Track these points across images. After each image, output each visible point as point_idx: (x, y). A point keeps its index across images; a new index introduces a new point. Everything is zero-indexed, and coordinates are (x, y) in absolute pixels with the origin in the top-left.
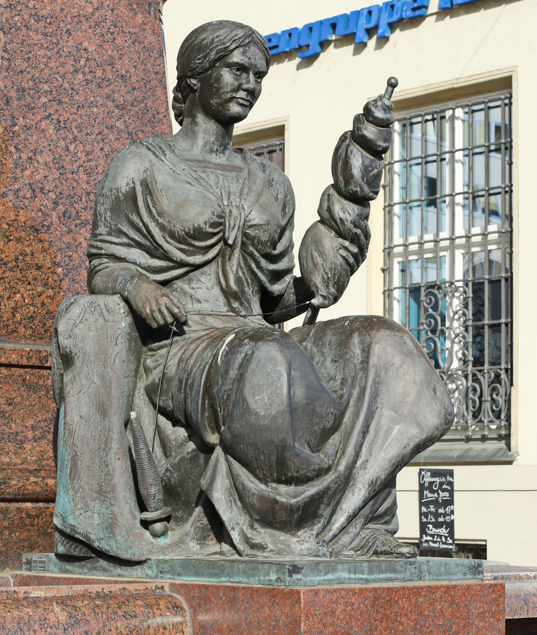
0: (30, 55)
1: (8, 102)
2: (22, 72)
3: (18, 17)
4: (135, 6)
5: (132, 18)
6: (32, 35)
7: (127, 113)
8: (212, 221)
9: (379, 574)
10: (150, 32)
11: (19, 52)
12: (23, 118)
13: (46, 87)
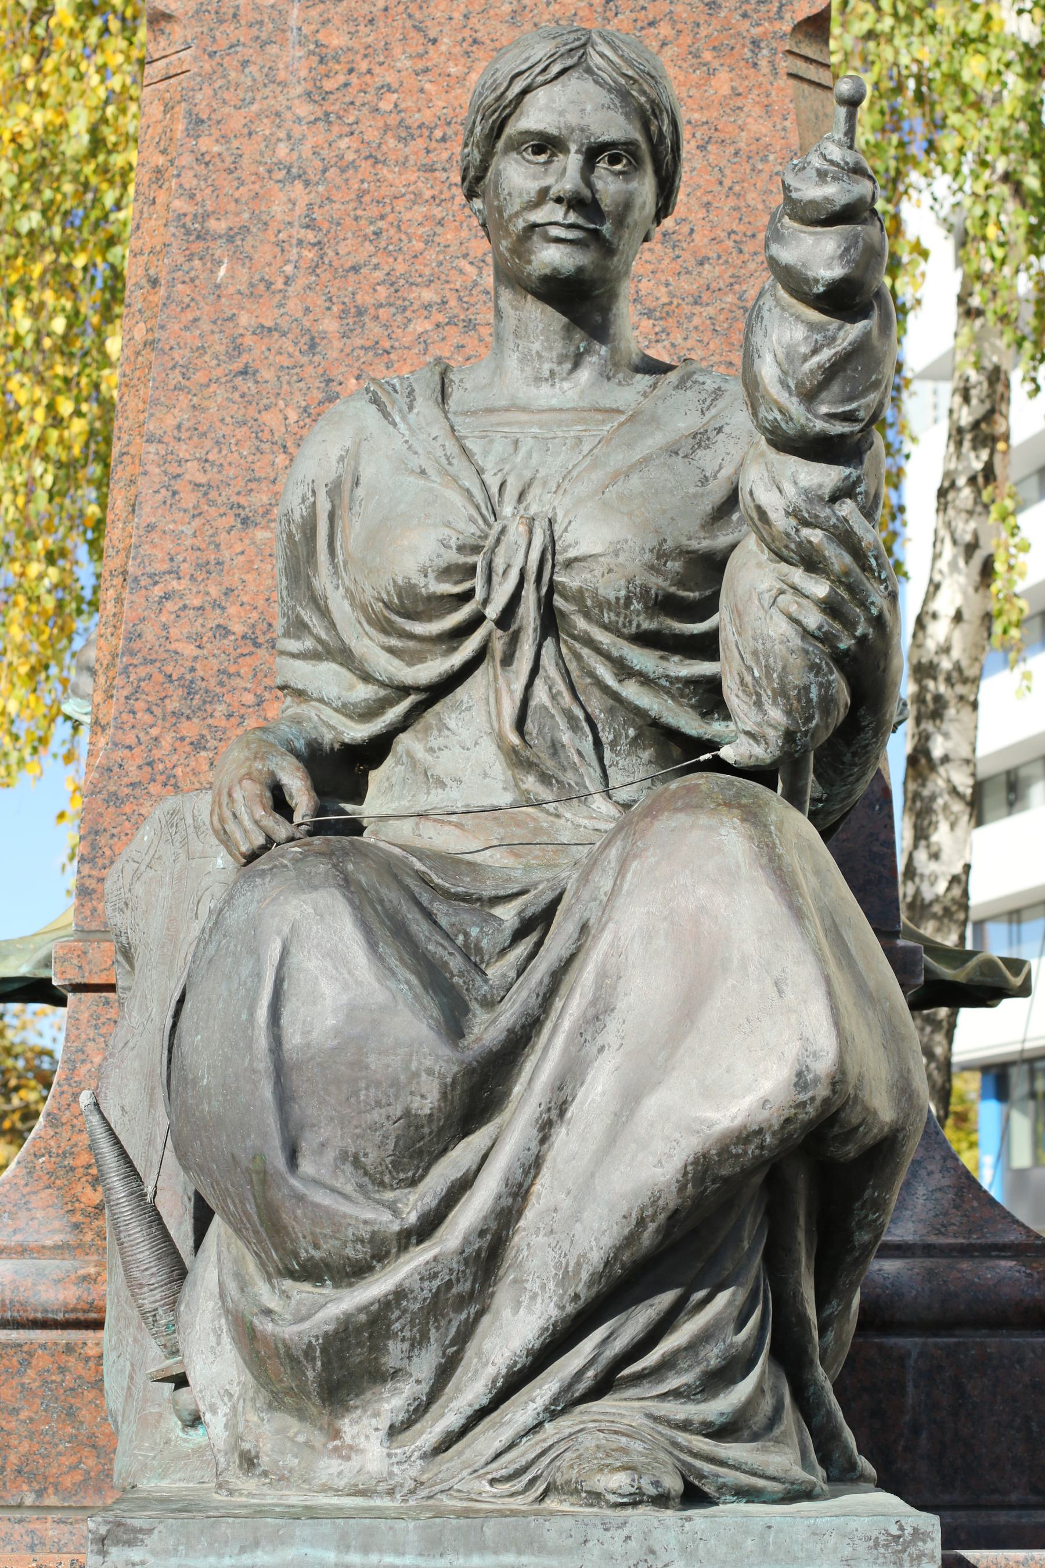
0: (381, 224)
1: (313, 346)
2: (355, 269)
3: (347, 140)
4: (707, 56)
5: (698, 86)
6: (390, 176)
7: (679, 324)
8: (442, 563)
9: (469, 1553)
10: (757, 111)
11: (349, 221)
12: (358, 378)
13: (428, 295)
